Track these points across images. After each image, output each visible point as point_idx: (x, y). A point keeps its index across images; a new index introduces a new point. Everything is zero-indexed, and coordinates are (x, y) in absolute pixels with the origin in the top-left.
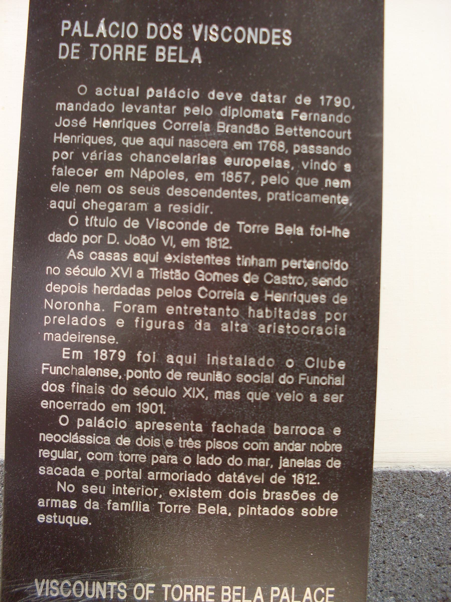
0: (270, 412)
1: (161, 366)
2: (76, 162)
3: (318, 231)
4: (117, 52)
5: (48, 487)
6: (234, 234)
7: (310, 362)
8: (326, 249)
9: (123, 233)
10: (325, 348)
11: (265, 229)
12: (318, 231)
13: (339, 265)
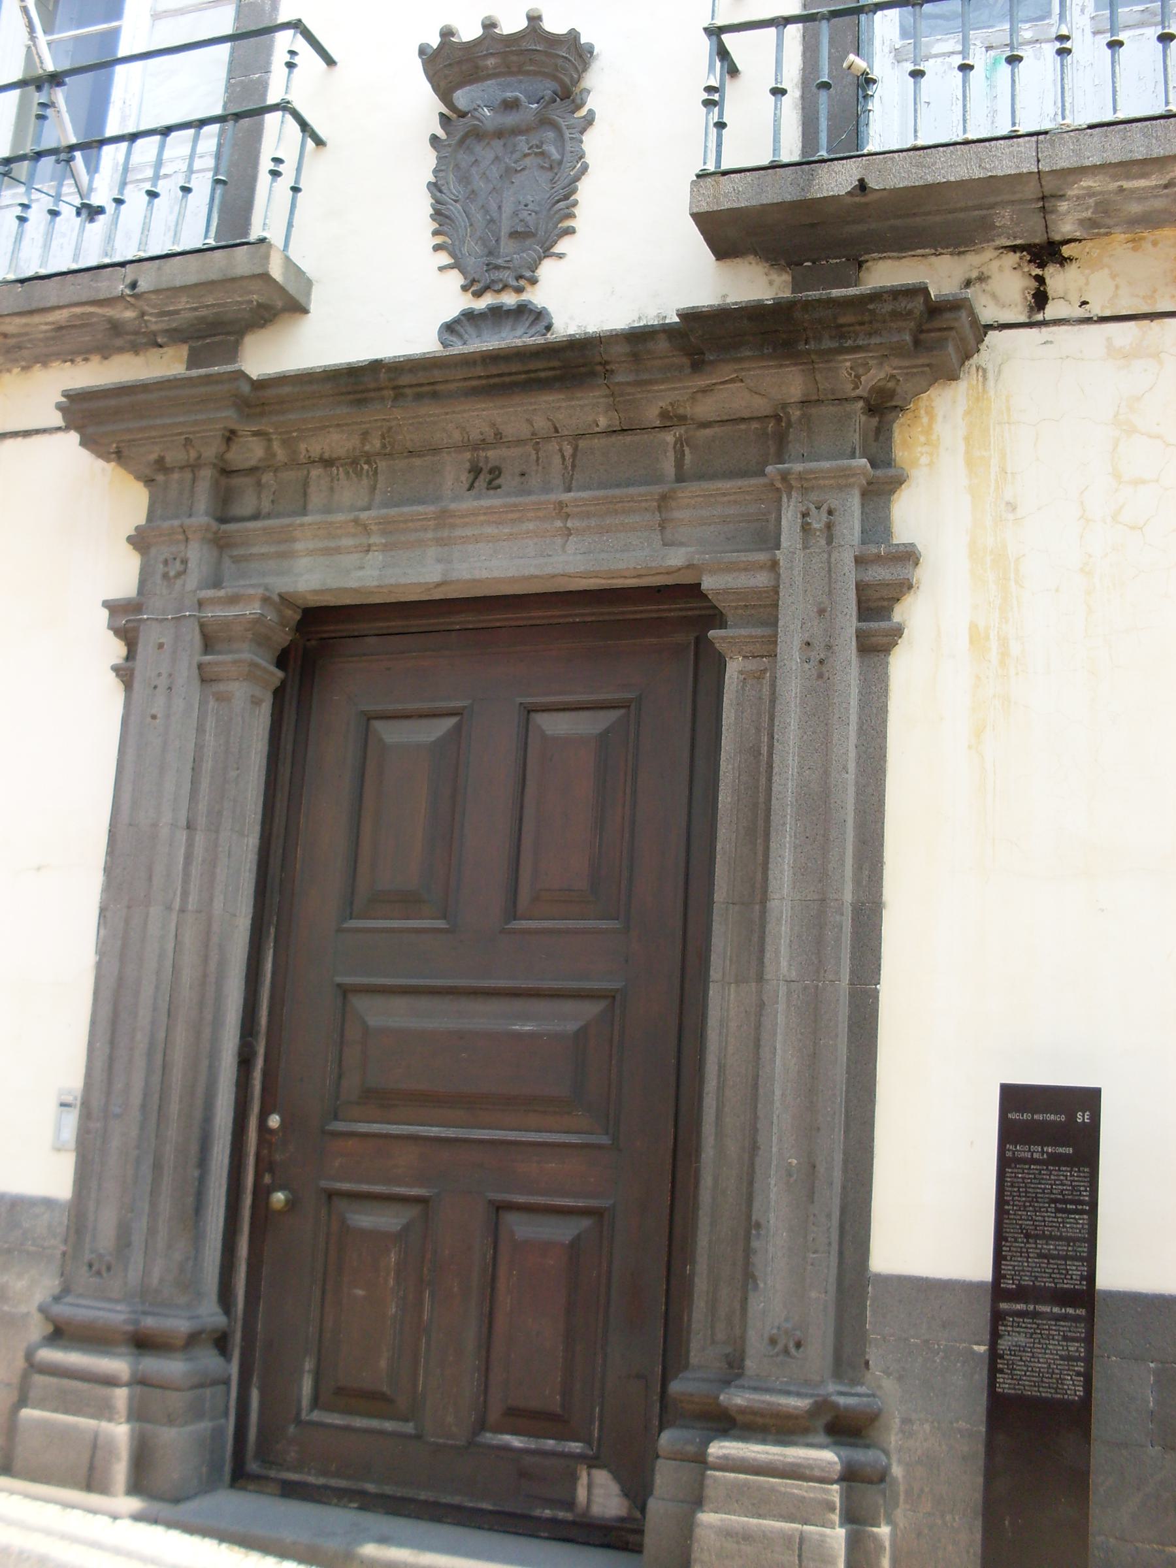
0: (1066, 1258)
1: (1036, 1243)
2: (1012, 1186)
3: (1080, 1207)
4: (1022, 1155)
5: (1004, 1277)
6: (1056, 1208)
7: (1078, 1244)
8: (1082, 1212)
9: (1025, 1206)
10: (1083, 1240)
11: (1036, 1117)
12: (1080, 1207)
13: (1086, 1217)
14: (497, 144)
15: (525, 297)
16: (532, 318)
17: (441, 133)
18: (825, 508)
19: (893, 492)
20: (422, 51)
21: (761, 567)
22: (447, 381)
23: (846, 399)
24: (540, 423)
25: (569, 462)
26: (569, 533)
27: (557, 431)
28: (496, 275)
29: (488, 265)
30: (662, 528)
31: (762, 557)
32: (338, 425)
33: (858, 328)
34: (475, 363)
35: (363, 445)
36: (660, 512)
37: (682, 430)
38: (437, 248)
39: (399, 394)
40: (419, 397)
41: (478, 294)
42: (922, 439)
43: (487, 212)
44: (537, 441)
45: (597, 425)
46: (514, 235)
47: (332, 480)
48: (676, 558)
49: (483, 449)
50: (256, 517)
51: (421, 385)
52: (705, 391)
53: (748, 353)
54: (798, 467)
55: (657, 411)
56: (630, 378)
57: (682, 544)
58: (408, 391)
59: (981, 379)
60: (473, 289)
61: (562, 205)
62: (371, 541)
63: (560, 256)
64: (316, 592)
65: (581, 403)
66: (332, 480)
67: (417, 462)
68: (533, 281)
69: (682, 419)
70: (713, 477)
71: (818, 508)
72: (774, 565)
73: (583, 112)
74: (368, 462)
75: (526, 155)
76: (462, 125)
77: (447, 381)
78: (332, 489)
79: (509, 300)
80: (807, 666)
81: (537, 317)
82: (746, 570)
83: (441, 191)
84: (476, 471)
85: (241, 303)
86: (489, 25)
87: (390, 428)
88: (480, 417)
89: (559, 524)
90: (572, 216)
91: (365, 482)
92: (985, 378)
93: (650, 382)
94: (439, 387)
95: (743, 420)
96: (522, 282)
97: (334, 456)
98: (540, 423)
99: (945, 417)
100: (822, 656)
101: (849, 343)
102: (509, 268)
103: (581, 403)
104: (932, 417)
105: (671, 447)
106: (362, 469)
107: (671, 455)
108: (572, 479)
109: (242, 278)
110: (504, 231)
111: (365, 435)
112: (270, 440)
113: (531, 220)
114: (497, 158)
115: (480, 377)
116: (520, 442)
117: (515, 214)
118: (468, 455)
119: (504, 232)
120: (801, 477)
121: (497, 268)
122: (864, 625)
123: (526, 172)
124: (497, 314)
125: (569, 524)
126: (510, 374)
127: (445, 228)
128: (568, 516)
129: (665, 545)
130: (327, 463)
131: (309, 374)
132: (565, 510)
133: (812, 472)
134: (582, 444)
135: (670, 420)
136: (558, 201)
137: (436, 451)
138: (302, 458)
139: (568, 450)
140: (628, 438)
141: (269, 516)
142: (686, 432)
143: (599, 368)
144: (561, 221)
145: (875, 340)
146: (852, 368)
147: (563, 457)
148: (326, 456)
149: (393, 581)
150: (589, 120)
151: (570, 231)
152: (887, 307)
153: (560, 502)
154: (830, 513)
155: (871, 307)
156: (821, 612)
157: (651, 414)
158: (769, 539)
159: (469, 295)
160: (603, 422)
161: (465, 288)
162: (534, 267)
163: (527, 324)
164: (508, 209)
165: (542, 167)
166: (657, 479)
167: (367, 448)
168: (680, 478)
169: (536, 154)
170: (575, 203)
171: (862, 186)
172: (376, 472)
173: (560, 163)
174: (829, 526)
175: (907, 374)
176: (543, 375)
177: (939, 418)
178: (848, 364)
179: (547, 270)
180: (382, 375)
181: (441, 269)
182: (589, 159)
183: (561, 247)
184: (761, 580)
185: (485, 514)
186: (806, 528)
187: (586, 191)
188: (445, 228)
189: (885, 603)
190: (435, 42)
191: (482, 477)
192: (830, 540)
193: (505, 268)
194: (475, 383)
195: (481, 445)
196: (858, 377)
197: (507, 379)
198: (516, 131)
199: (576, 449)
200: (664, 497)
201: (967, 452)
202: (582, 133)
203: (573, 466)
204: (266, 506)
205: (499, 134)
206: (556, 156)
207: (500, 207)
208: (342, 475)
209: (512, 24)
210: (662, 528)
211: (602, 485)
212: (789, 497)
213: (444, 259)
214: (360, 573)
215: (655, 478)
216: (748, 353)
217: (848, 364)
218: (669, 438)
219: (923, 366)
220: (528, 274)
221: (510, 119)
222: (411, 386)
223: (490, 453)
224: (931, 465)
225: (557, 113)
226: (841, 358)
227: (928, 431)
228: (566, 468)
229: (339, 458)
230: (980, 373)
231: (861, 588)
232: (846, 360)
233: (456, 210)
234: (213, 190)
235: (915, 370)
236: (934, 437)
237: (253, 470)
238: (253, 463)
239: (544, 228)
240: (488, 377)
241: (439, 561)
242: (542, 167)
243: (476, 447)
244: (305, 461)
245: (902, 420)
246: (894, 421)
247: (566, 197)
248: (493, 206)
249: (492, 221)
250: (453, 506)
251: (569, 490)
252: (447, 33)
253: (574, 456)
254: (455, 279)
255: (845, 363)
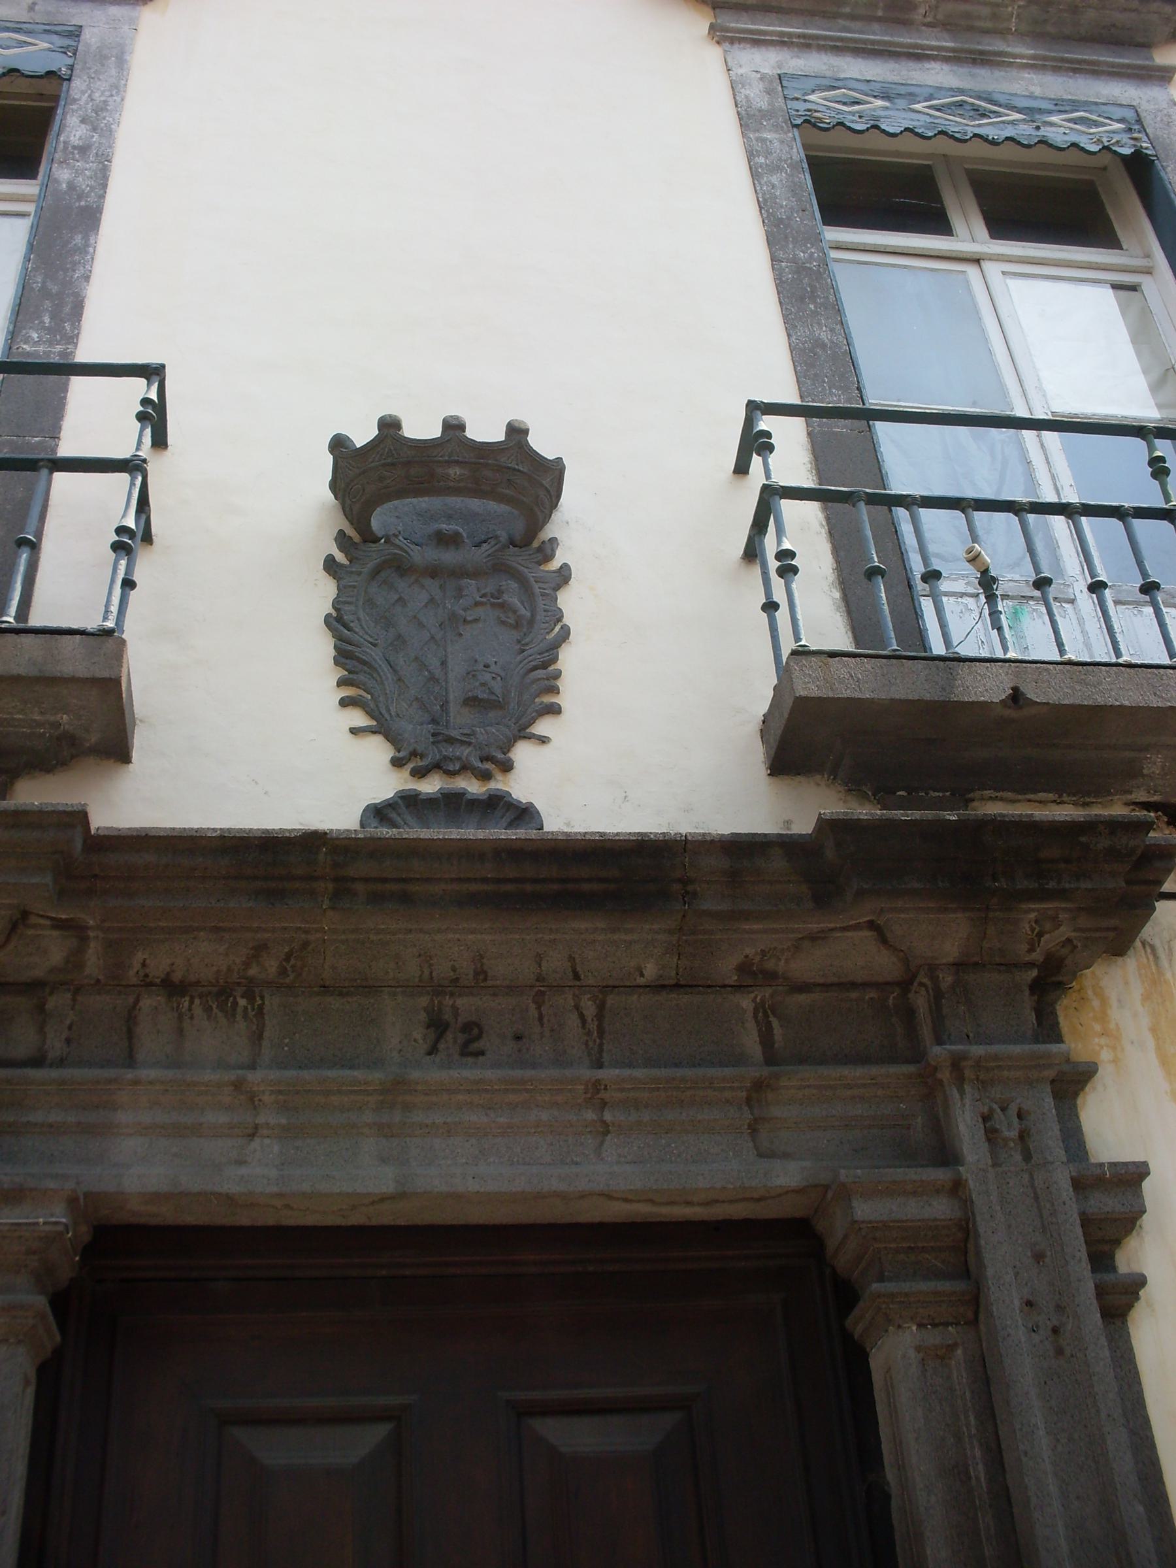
14: (433, 585)
15: (493, 785)
16: (509, 816)
17: (340, 557)
18: (1013, 1110)
19: (1076, 1095)
20: (339, 444)
21: (938, 1191)
22: (428, 880)
23: (1015, 965)
24: (555, 962)
25: (593, 1026)
26: (605, 1130)
27: (577, 976)
28: (449, 751)
29: (433, 735)
30: (753, 1130)
31: (941, 1175)
32: (216, 929)
33: (1063, 866)
34: (482, 856)
35: (247, 965)
36: (750, 1107)
37: (768, 991)
38: (344, 703)
39: (342, 890)
40: (376, 899)
41: (419, 773)
42: (1098, 1027)
43: (423, 666)
44: (541, 989)
45: (642, 975)
46: (471, 702)
47: (180, 1017)
48: (787, 1175)
49: (452, 995)
50: (38, 1061)
51: (384, 880)
52: (815, 938)
53: (917, 885)
54: (977, 1050)
55: (734, 961)
56: (724, 906)
57: (786, 1156)
58: (360, 887)
59: (1151, 957)
60: (410, 766)
61: (540, 673)
62: (261, 1120)
63: (543, 740)
64: (156, 1197)
65: (628, 937)
66: (180, 1017)
67: (335, 1003)
68: (507, 767)
69: (771, 977)
70: (822, 1061)
71: (1003, 1109)
72: (957, 1188)
73: (555, 564)
74: (249, 996)
75: (477, 604)
76: (374, 555)
77: (428, 880)
78: (180, 1032)
79: (473, 787)
80: (1036, 1338)
81: (525, 814)
82: (914, 1193)
83: (345, 626)
84: (437, 1026)
85: (39, 724)
86: (454, 427)
87: (306, 944)
88: (456, 942)
89: (590, 1115)
90: (555, 690)
91: (242, 1025)
92: (1156, 958)
93: (746, 916)
94: (413, 888)
95: (854, 985)
96: (488, 766)
97: (192, 978)
98: (555, 962)
99: (1119, 1001)
100: (1056, 1323)
101: (1052, 885)
102: (470, 744)
103: (628, 937)
104: (1104, 1001)
105: (749, 1015)
106: (235, 1003)
107: (751, 1025)
108: (601, 1051)
109: (73, 680)
110: (455, 693)
111: (260, 949)
112: (84, 940)
113: (497, 686)
114: (432, 600)
115: (485, 880)
116: (512, 989)
117: (471, 674)
118: (424, 1001)
119: (455, 693)
120: (978, 1064)
121: (450, 740)
122: (1099, 1276)
123: (480, 625)
124: (452, 805)
125: (608, 1116)
126: (535, 881)
127: (362, 677)
128: (604, 1104)
129: (761, 1155)
130: (173, 988)
131: (192, 838)
132: (602, 1095)
133: (996, 1057)
134: (611, 1000)
135: (752, 975)
136: (535, 668)
137: (369, 988)
138: (132, 976)
139: (590, 1009)
140: (685, 999)
141: (61, 1063)
142: (772, 996)
143: (676, 887)
144: (538, 696)
145: (1085, 885)
146: (1036, 922)
147: (582, 1017)
148: (177, 977)
149: (306, 1187)
150: (564, 576)
151: (554, 710)
152: (1104, 843)
153: (598, 1081)
154: (1020, 1116)
155: (1083, 839)
156: (1039, 1257)
157: (726, 966)
158: (945, 1154)
159: (405, 773)
160: (651, 971)
161: (397, 763)
162: (507, 747)
163: (504, 822)
164: (457, 668)
165: (503, 623)
166: (739, 1059)
167: (253, 971)
168: (771, 1058)
169: (493, 605)
170: (558, 675)
171: (1016, 696)
172: (260, 1012)
173: (531, 622)
174: (1023, 1136)
175: (1087, 938)
176: (586, 887)
177: (1113, 1002)
178: (1033, 915)
179: (522, 753)
180: (321, 857)
181: (354, 731)
182: (566, 620)
183: (542, 727)
184: (941, 1209)
185: (469, 1092)
186: (992, 1135)
187: (569, 660)
188: (362, 677)
189: (1106, 1248)
190: (363, 434)
191: (449, 1036)
192: (1027, 1156)
193: (462, 743)
194: (474, 887)
195: (455, 985)
196: (1040, 935)
197: (529, 887)
198: (459, 573)
199: (601, 1007)
200: (759, 1086)
201: (1158, 1048)
202: (558, 587)
203: (601, 1032)
204: (55, 1045)
205: (434, 572)
206: (525, 612)
207: (444, 663)
208: (198, 1010)
209: (485, 429)
210: (753, 1130)
211: (649, 1063)
212: (962, 1093)
213: (358, 718)
214: (243, 1170)
215: (739, 1059)
216: (917, 885)
217: (1033, 915)
218: (746, 1002)
219: (1108, 929)
220: (500, 756)
221: (449, 557)
222: (367, 880)
223: (460, 1002)
224: (1115, 1061)
225: (516, 559)
226: (1024, 906)
227: (1103, 1018)
228: (589, 1033)
229: (198, 983)
230: (1149, 951)
231: (1086, 1222)
232: (1033, 910)
233: (375, 655)
234: (39, 534)
235: (1097, 935)
236: (1112, 1026)
237: (34, 987)
238: (38, 973)
239: (522, 696)
240: (498, 881)
241: (384, 1160)
242: (503, 623)
243: (439, 990)
244: (134, 981)
245: (1065, 1002)
246: (1059, 998)
247: (545, 665)
248: (434, 663)
249: (433, 678)
250: (415, 1075)
251: (600, 1065)
252: (389, 426)
253: (600, 1016)
254: (378, 751)
255: (1029, 914)
